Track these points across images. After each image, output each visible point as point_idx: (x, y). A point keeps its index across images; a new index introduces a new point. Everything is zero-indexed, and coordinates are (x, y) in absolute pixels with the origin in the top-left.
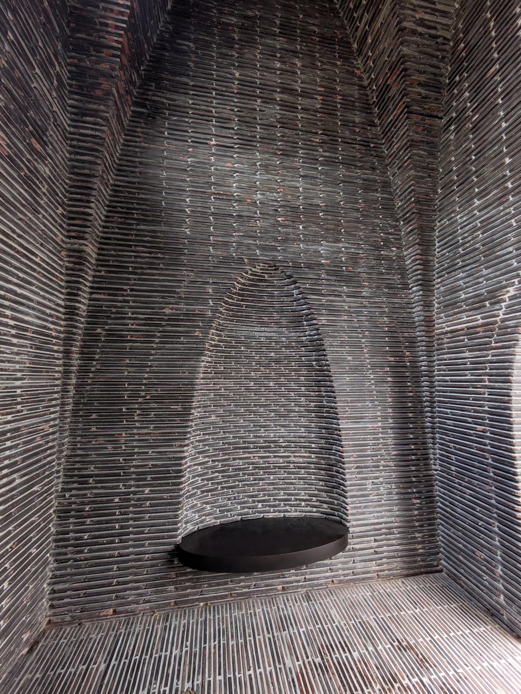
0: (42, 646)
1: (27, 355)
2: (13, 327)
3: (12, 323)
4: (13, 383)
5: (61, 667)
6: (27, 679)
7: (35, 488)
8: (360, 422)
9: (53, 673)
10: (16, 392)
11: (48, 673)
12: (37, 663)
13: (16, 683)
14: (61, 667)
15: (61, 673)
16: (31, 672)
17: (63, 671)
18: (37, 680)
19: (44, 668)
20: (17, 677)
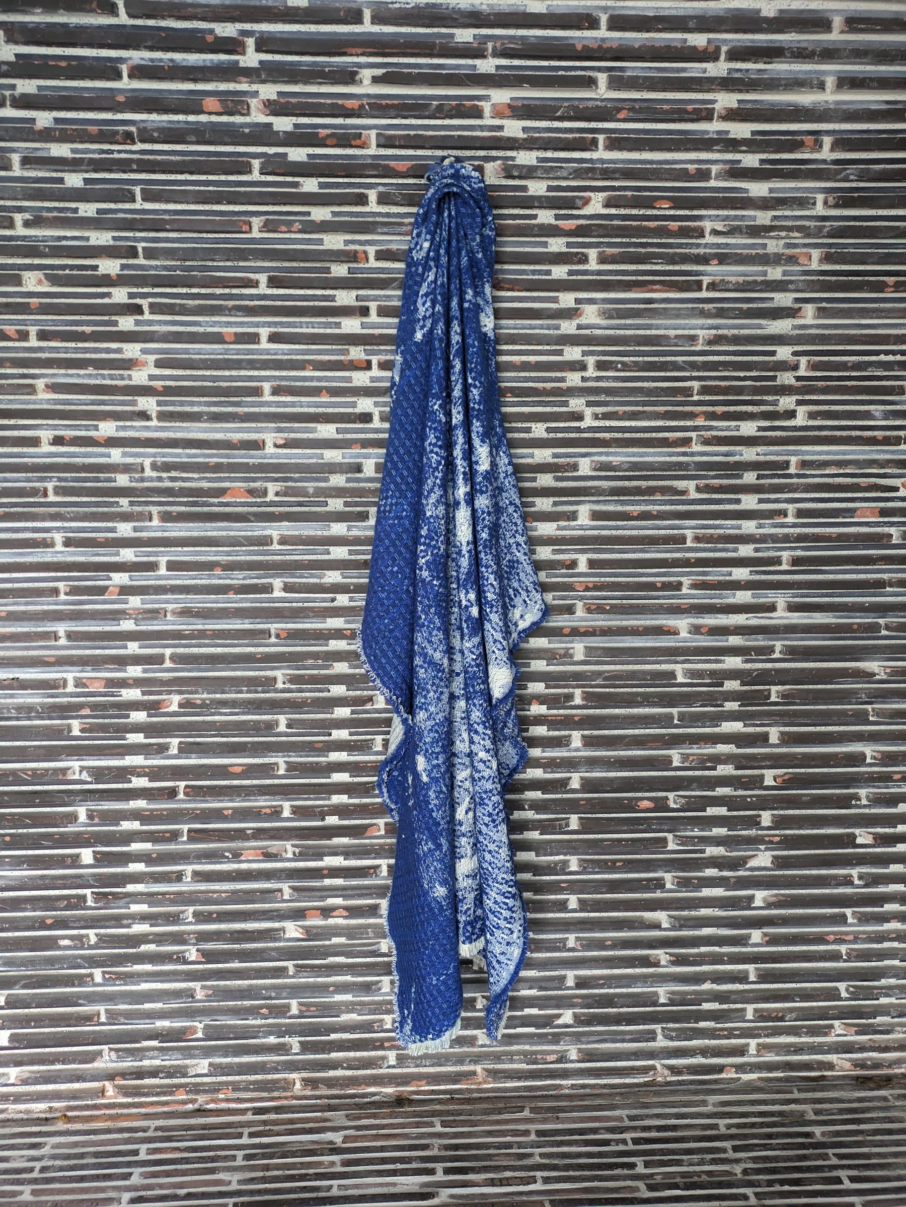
0: (885, 1099)
1: (799, 229)
2: (751, 145)
3: (742, 130)
4: (760, 327)
5: (854, 1173)
6: (802, 1114)
7: (872, 666)
8: (651, 491)
9: (835, 1161)
10: (773, 353)
11: (830, 1152)
12: (841, 1111)
13: (788, 1096)
14: (854, 1173)
15: (841, 1182)
16: (817, 1112)
17: (847, 1185)
18: (808, 1135)
19: (838, 1134)
20: (800, 1090)
